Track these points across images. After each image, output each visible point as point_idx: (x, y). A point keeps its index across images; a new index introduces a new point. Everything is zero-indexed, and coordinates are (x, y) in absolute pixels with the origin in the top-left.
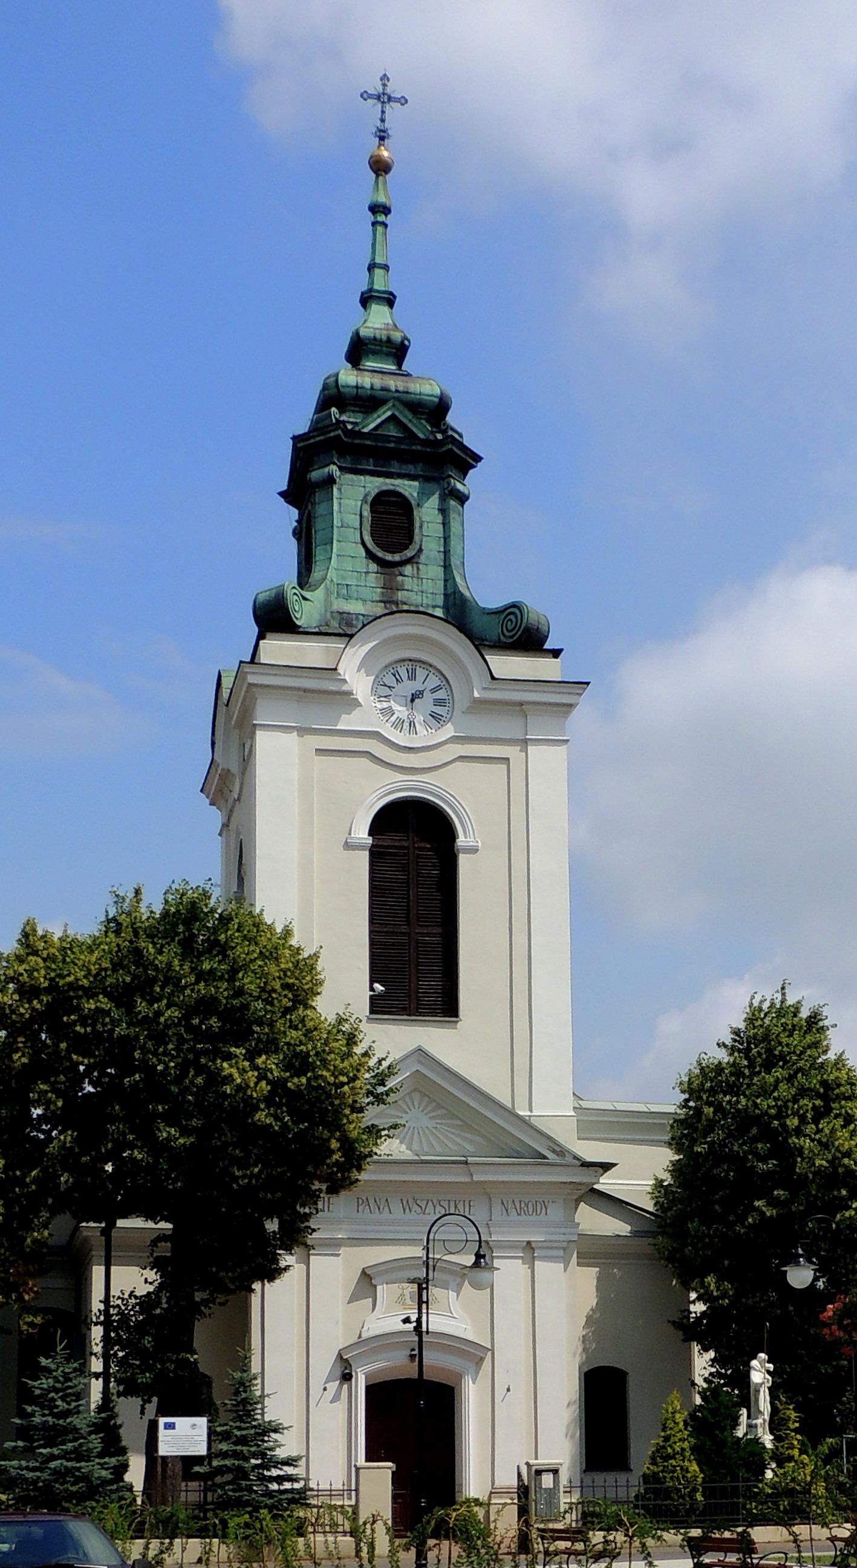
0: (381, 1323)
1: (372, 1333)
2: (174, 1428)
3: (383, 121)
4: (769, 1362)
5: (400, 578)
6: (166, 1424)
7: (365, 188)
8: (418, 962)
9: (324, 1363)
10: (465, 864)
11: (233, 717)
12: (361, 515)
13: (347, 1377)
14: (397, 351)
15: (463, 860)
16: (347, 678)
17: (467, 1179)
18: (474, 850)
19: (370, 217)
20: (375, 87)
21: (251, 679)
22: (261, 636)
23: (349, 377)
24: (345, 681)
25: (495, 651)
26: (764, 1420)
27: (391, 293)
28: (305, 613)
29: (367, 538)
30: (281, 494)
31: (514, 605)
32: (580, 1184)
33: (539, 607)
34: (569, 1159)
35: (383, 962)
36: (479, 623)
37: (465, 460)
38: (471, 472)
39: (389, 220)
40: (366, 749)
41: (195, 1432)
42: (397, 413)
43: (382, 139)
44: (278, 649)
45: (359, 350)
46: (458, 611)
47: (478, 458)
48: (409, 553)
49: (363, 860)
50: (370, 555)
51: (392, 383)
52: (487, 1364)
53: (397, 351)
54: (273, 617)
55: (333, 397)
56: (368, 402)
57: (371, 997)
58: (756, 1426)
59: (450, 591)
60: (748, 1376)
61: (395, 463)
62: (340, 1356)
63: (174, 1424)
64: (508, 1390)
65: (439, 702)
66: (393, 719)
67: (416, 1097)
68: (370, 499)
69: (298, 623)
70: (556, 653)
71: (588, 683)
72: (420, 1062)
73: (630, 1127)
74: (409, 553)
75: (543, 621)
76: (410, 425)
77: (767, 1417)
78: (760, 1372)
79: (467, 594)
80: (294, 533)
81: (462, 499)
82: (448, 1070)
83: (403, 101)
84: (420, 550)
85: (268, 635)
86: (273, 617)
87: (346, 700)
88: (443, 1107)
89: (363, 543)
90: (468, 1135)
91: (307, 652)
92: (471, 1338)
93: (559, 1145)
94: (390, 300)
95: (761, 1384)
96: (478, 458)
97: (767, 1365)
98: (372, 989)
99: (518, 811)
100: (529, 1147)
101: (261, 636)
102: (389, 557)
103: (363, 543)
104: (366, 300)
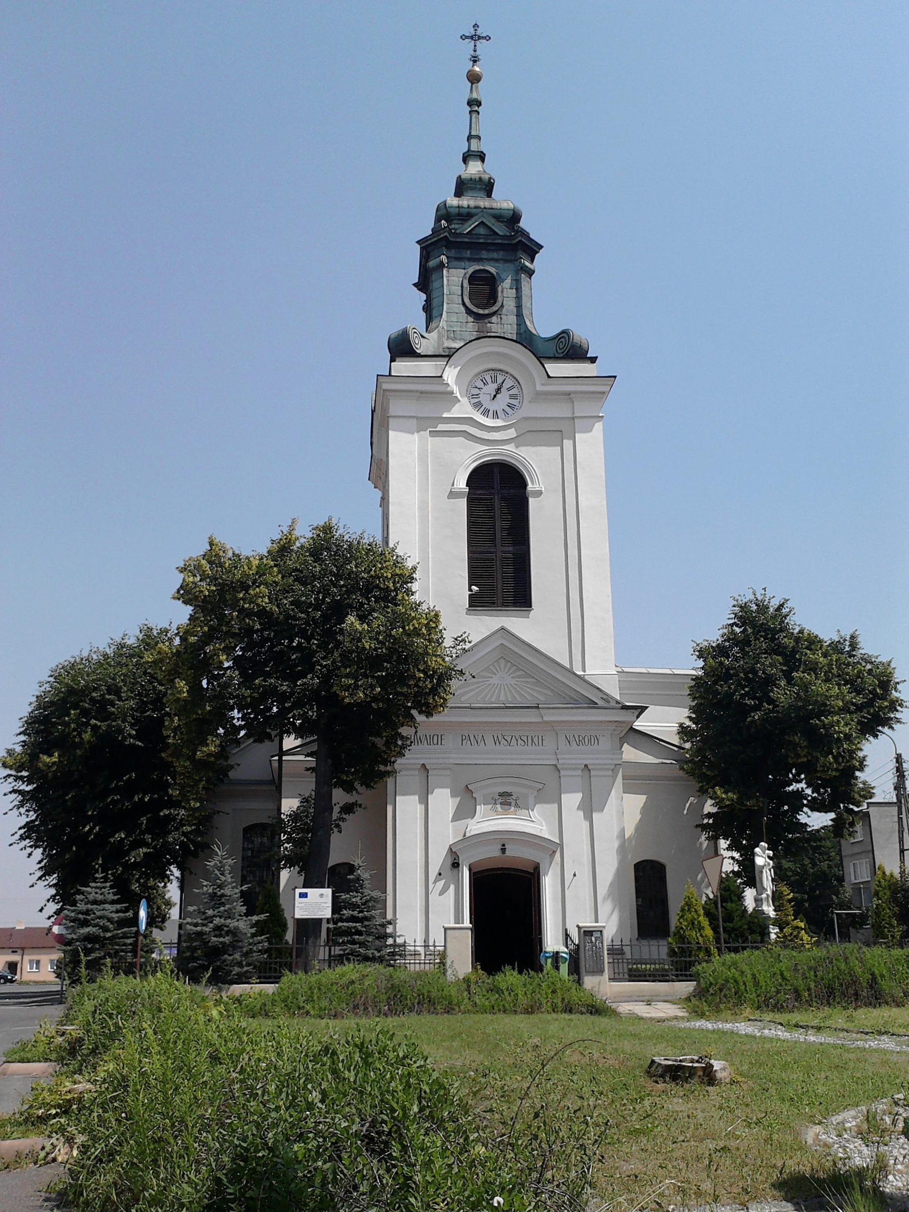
0: (479, 825)
1: (473, 833)
2: (306, 897)
3: (475, 51)
4: (769, 849)
5: (489, 325)
6: (300, 894)
7: (464, 90)
8: (501, 567)
9: (438, 857)
10: (533, 504)
11: (379, 424)
12: (462, 287)
13: (456, 865)
14: (487, 187)
15: (532, 501)
16: (449, 382)
17: (540, 720)
18: (539, 493)
19: (468, 109)
20: (470, 31)
21: (385, 386)
22: (392, 360)
23: (453, 201)
24: (448, 384)
25: (551, 361)
26: (768, 895)
27: (482, 152)
28: (422, 346)
29: (467, 301)
30: (414, 285)
31: (563, 332)
32: (623, 722)
33: (580, 334)
34: (613, 704)
35: (478, 570)
36: (540, 346)
37: (532, 249)
38: (537, 255)
39: (480, 109)
40: (464, 431)
41: (322, 900)
42: (485, 221)
43: (475, 61)
44: (403, 367)
45: (462, 186)
46: (526, 339)
47: (542, 247)
48: (495, 308)
49: (463, 503)
50: (469, 312)
51: (484, 203)
52: (558, 855)
53: (487, 187)
54: (401, 347)
55: (444, 214)
56: (465, 215)
57: (470, 595)
58: (761, 900)
59: (522, 331)
60: (754, 862)
61: (484, 252)
62: (450, 849)
63: (306, 894)
64: (575, 875)
65: (513, 397)
66: (482, 409)
67: (502, 662)
68: (468, 276)
69: (418, 351)
70: (593, 360)
71: (615, 377)
72: (503, 637)
73: (661, 688)
74: (495, 308)
75: (584, 341)
76: (494, 228)
77: (769, 892)
78: (762, 857)
79: (534, 332)
80: (423, 309)
81: (530, 273)
82: (523, 642)
83: (488, 38)
84: (502, 306)
85: (397, 359)
86: (401, 347)
87: (448, 398)
88: (521, 670)
89: (464, 304)
90: (539, 689)
91: (426, 368)
92: (547, 836)
93: (607, 695)
94: (482, 157)
95: (763, 867)
96: (542, 247)
97: (767, 852)
98: (470, 590)
99: (569, 466)
100: (587, 698)
101: (392, 360)
102: (481, 312)
103: (464, 304)
104: (466, 158)
